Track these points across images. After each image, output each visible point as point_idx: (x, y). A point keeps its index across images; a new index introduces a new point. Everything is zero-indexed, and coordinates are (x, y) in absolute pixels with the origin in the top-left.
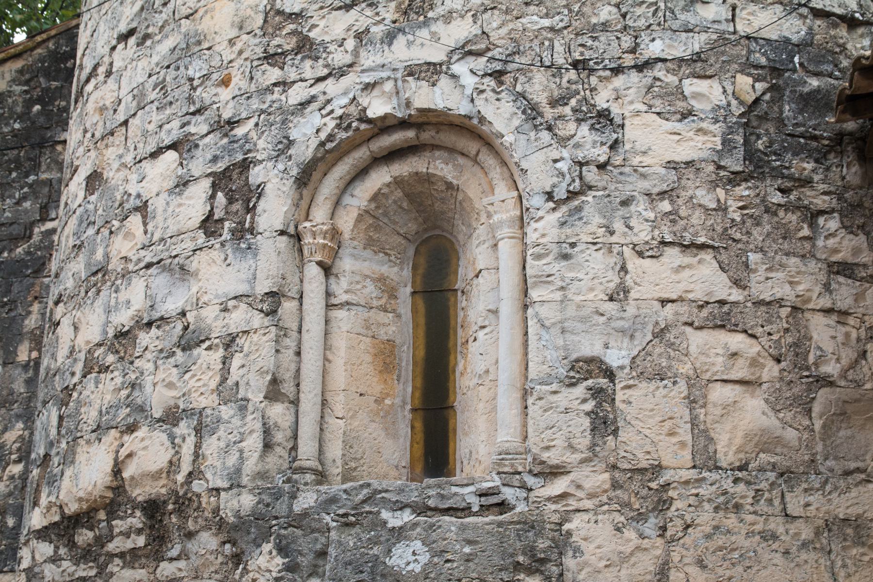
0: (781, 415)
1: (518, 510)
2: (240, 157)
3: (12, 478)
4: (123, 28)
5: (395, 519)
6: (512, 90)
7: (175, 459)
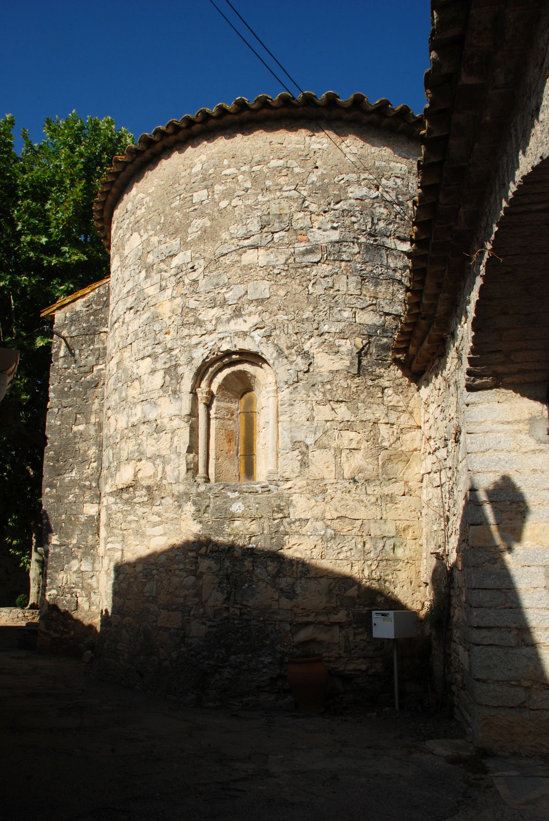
0: (367, 460)
1: (274, 493)
2: (174, 363)
3: (93, 468)
4: (129, 306)
5: (232, 495)
6: (273, 343)
7: (156, 472)
